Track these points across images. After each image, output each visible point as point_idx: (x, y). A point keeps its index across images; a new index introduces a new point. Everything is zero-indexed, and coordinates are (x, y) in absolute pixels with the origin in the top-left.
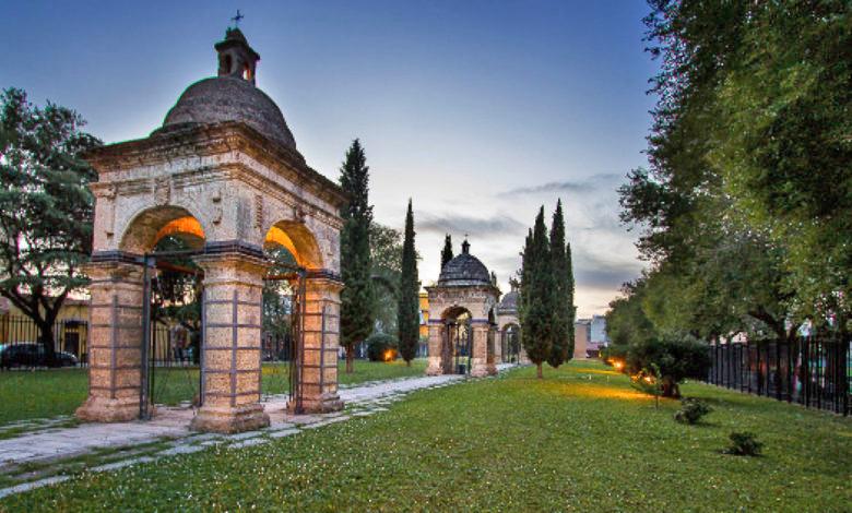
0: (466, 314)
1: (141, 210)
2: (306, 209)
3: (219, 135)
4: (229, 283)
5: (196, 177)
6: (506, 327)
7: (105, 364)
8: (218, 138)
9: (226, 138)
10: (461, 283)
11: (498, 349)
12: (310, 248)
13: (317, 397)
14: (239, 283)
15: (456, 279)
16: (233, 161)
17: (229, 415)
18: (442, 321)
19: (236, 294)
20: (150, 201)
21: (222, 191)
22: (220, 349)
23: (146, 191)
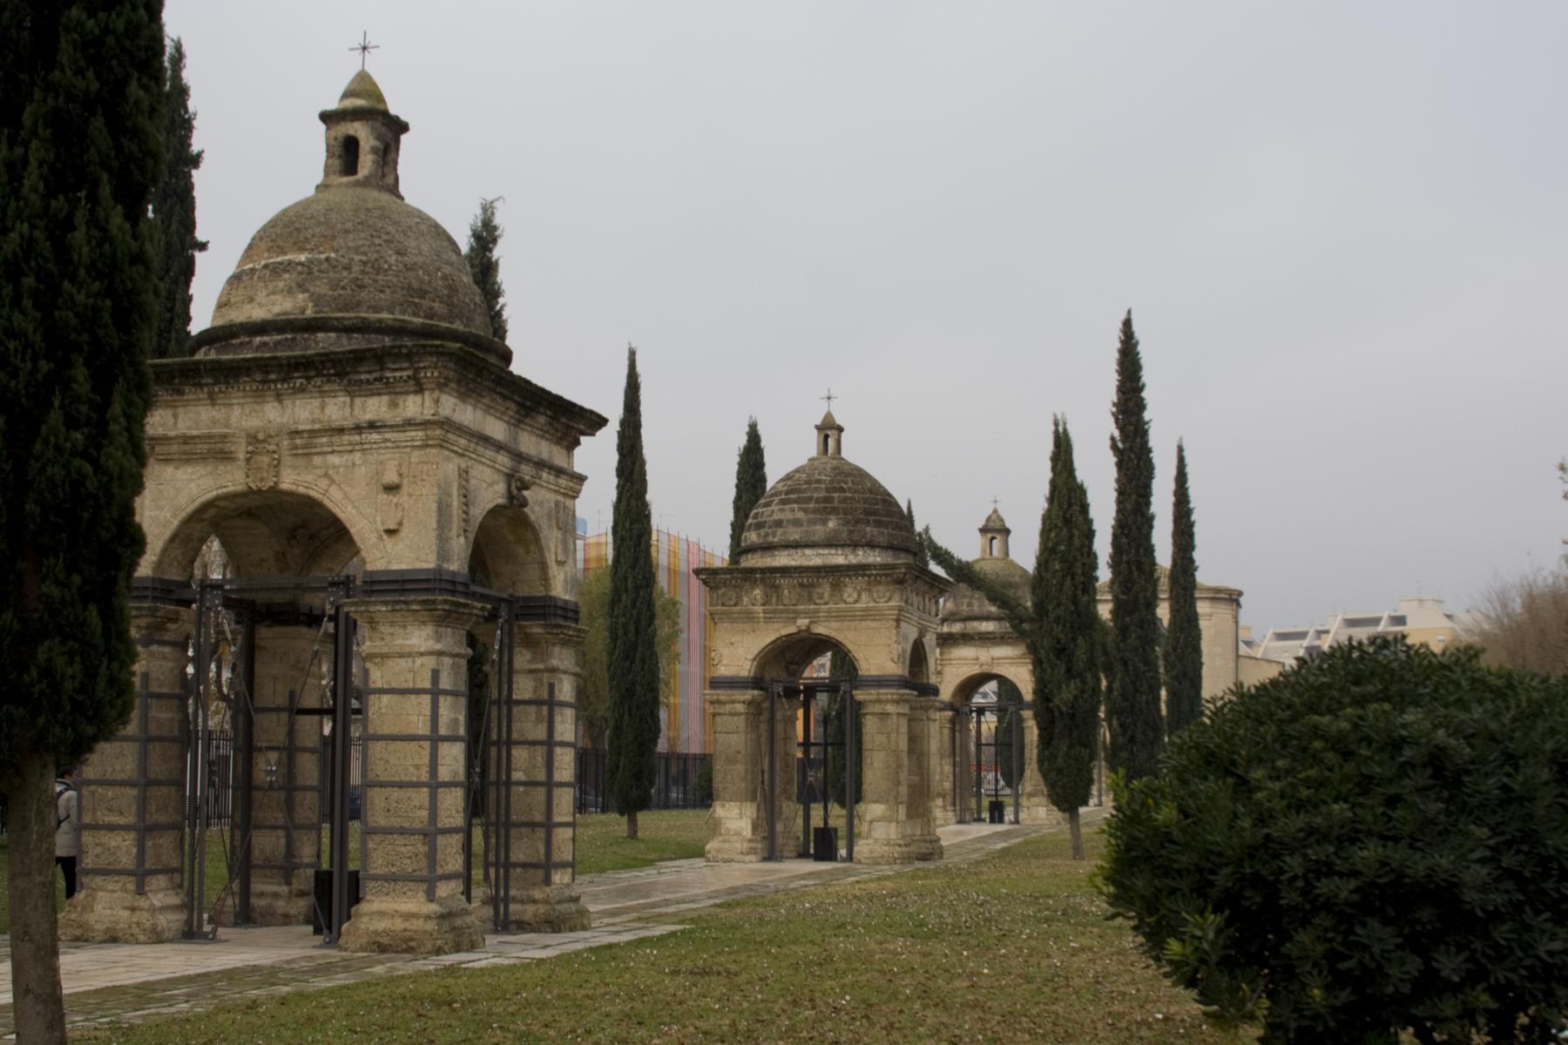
0: (826, 659)
1: (210, 496)
2: (527, 471)
3: (406, 365)
4: (422, 654)
5: (346, 438)
6: (970, 686)
7: (122, 821)
8: (402, 369)
9: (417, 370)
10: (814, 558)
11: (941, 771)
12: (521, 551)
13: (537, 894)
14: (440, 654)
15: (796, 546)
16: (428, 414)
17: (428, 917)
18: (757, 682)
19: (435, 674)
20: (232, 479)
21: (404, 470)
22: (401, 785)
23: (225, 457)
